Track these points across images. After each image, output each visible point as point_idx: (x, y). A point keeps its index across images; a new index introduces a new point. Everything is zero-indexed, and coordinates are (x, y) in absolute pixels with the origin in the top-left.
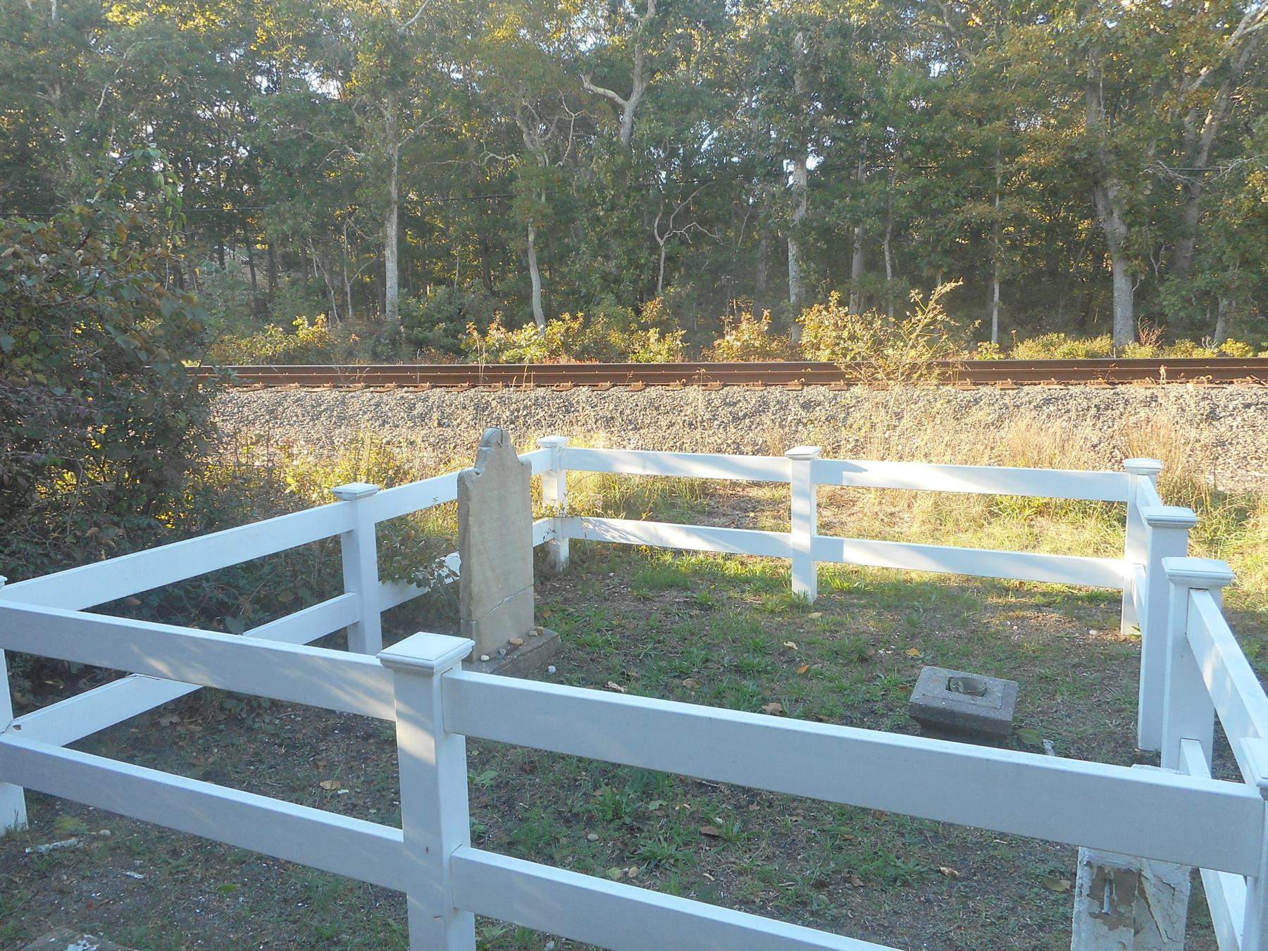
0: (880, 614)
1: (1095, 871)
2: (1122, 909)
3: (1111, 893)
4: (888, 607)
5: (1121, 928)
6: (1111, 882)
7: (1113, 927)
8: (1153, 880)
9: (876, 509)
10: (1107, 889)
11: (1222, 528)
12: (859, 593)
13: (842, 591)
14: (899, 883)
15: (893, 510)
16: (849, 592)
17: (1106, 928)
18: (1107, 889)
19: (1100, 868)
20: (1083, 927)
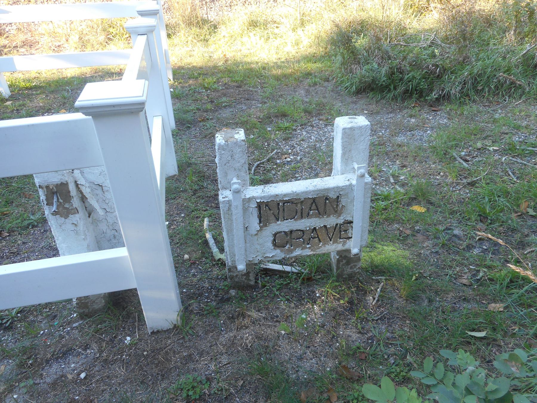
0: (47, 96)
1: (45, 189)
2: (67, 206)
3: (58, 199)
4: (52, 92)
5: (71, 216)
6: (56, 193)
7: (66, 217)
8: (87, 185)
9: (50, 44)
10: (55, 198)
11: (208, 33)
12: (36, 88)
13: (27, 88)
14: (30, 227)
15: (59, 44)
16: (31, 88)
17: (63, 219)
18: (55, 198)
19: (47, 187)
20: (52, 222)
